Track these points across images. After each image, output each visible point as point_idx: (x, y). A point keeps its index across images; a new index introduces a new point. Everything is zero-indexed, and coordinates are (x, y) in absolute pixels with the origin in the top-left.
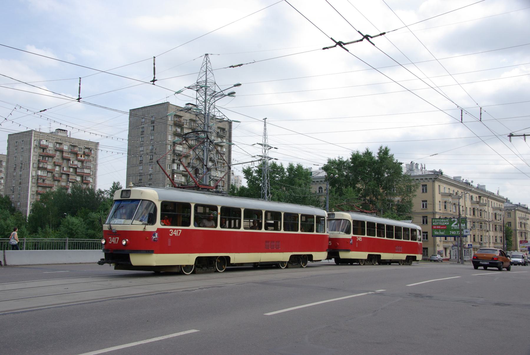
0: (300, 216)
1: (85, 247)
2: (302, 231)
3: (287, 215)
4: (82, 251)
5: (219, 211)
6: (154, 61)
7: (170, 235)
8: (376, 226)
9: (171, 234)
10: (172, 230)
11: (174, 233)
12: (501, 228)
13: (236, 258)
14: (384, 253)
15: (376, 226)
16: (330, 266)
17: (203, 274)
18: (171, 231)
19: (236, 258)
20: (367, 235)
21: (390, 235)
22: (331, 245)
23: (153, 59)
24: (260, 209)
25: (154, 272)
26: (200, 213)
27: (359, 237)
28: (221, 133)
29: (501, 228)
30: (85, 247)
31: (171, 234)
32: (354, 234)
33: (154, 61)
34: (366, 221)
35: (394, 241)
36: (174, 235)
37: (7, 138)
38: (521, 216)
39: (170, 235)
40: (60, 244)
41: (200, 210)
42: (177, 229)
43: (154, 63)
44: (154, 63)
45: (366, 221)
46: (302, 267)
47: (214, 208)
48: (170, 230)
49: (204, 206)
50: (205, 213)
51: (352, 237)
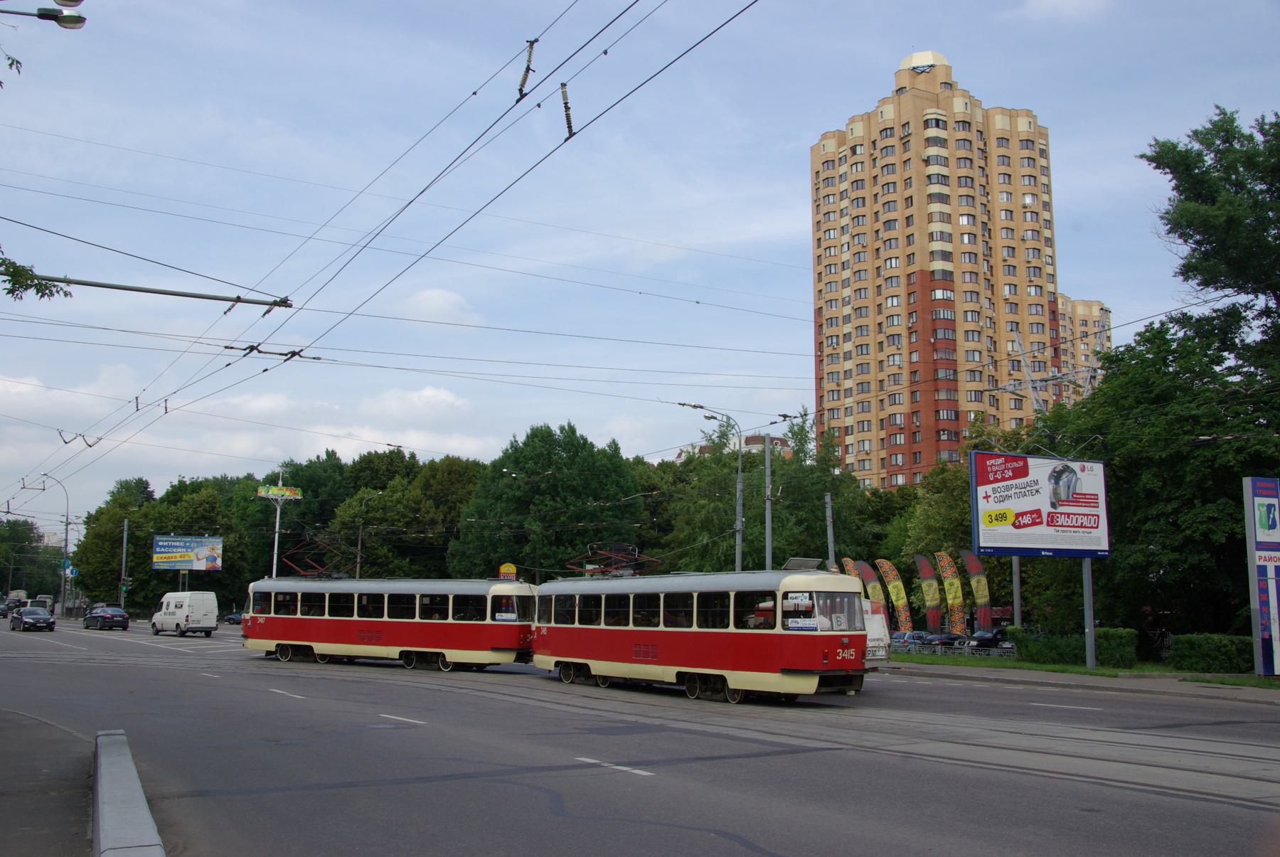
0: (418, 597)
2: (607, 624)
3: (610, 598)
5: (299, 598)
6: (565, 95)
7: (838, 658)
8: (577, 602)
11: (844, 655)
13: (320, 648)
15: (577, 602)
16: (507, 671)
19: (320, 648)
20: (700, 626)
21: (544, 616)
22: (853, 658)
24: (350, 592)
26: (281, 601)
27: (262, 618)
32: (539, 621)
33: (565, 95)
34: (695, 592)
35: (328, 620)
36: (843, 658)
37: (1030, 471)
38: (158, 549)
39: (838, 658)
41: (280, 598)
43: (566, 104)
44: (566, 104)
45: (695, 592)
46: (599, 686)
47: (294, 595)
49: (285, 594)
50: (284, 600)
51: (251, 617)
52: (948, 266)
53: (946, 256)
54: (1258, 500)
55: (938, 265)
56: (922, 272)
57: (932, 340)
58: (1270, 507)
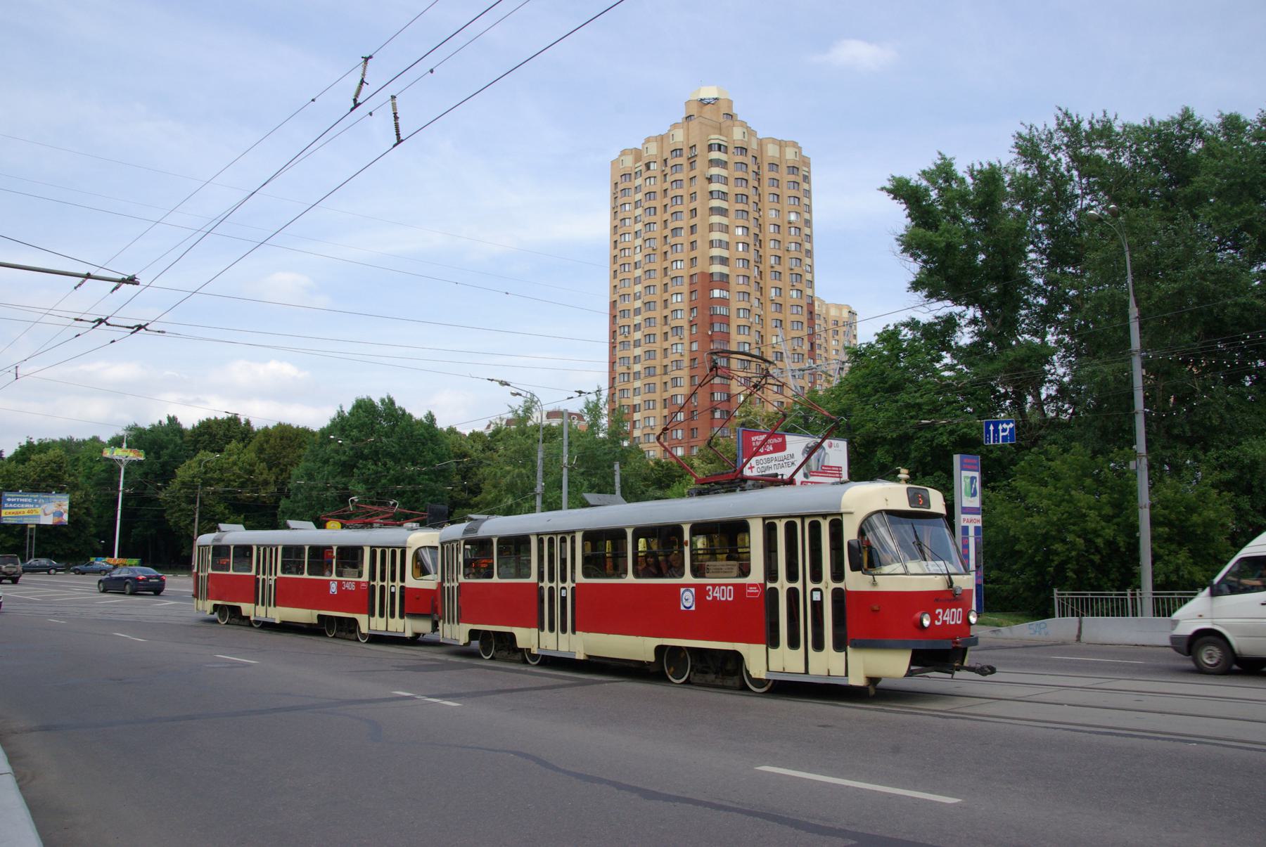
1: (1113, 611)
2: (234, 570)
4: (1139, 620)
9: (709, 596)
10: (711, 588)
12: (854, 824)
14: (584, 631)
17: (919, 690)
18: (709, 590)
23: (390, 102)
25: (1239, 669)
28: (639, 173)
29: (854, 824)
30: (1113, 611)
31: (709, 596)
37: (788, 446)
40: (1082, 610)
42: (720, 585)
43: (395, 114)
44: (395, 114)
48: (708, 588)
52: (725, 270)
53: (724, 261)
54: (965, 473)
55: (717, 268)
56: (703, 274)
57: (710, 333)
58: (973, 478)
